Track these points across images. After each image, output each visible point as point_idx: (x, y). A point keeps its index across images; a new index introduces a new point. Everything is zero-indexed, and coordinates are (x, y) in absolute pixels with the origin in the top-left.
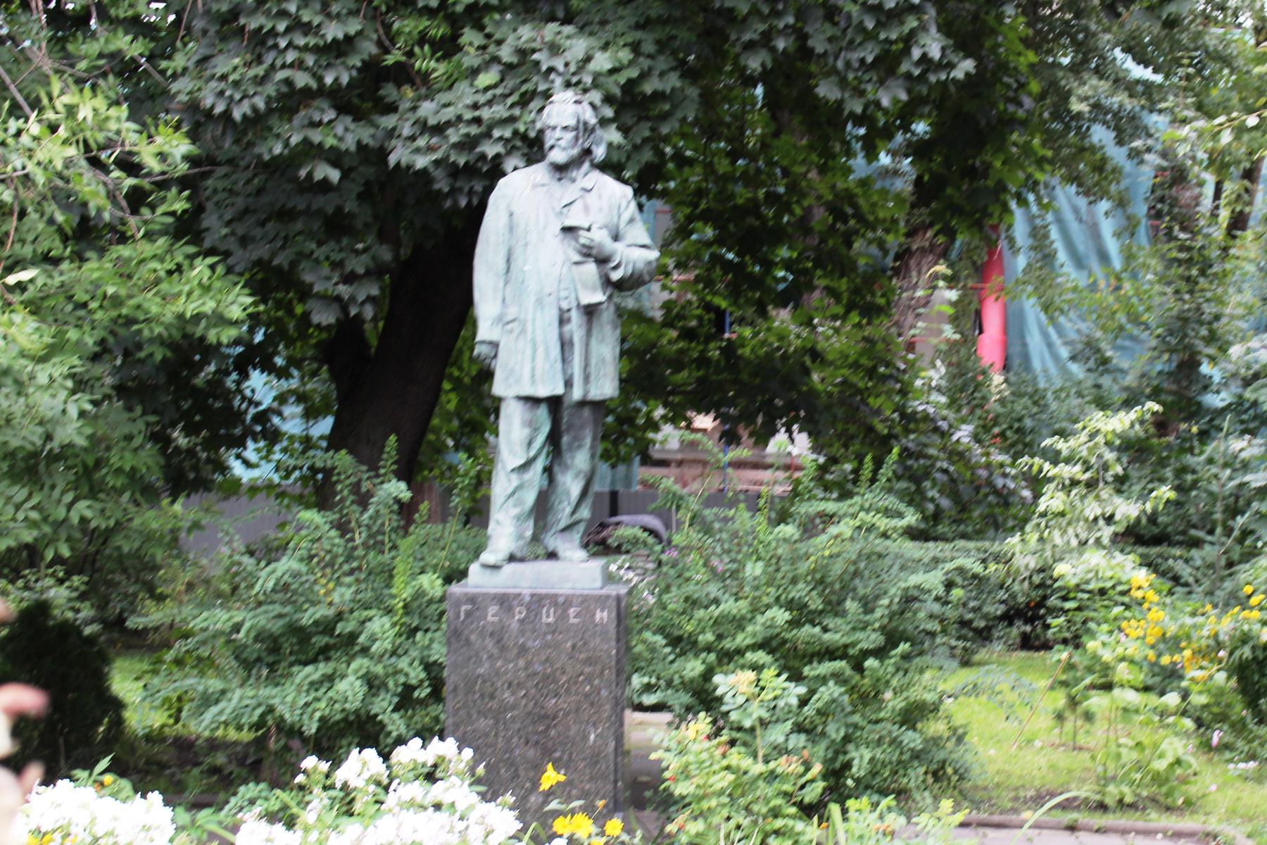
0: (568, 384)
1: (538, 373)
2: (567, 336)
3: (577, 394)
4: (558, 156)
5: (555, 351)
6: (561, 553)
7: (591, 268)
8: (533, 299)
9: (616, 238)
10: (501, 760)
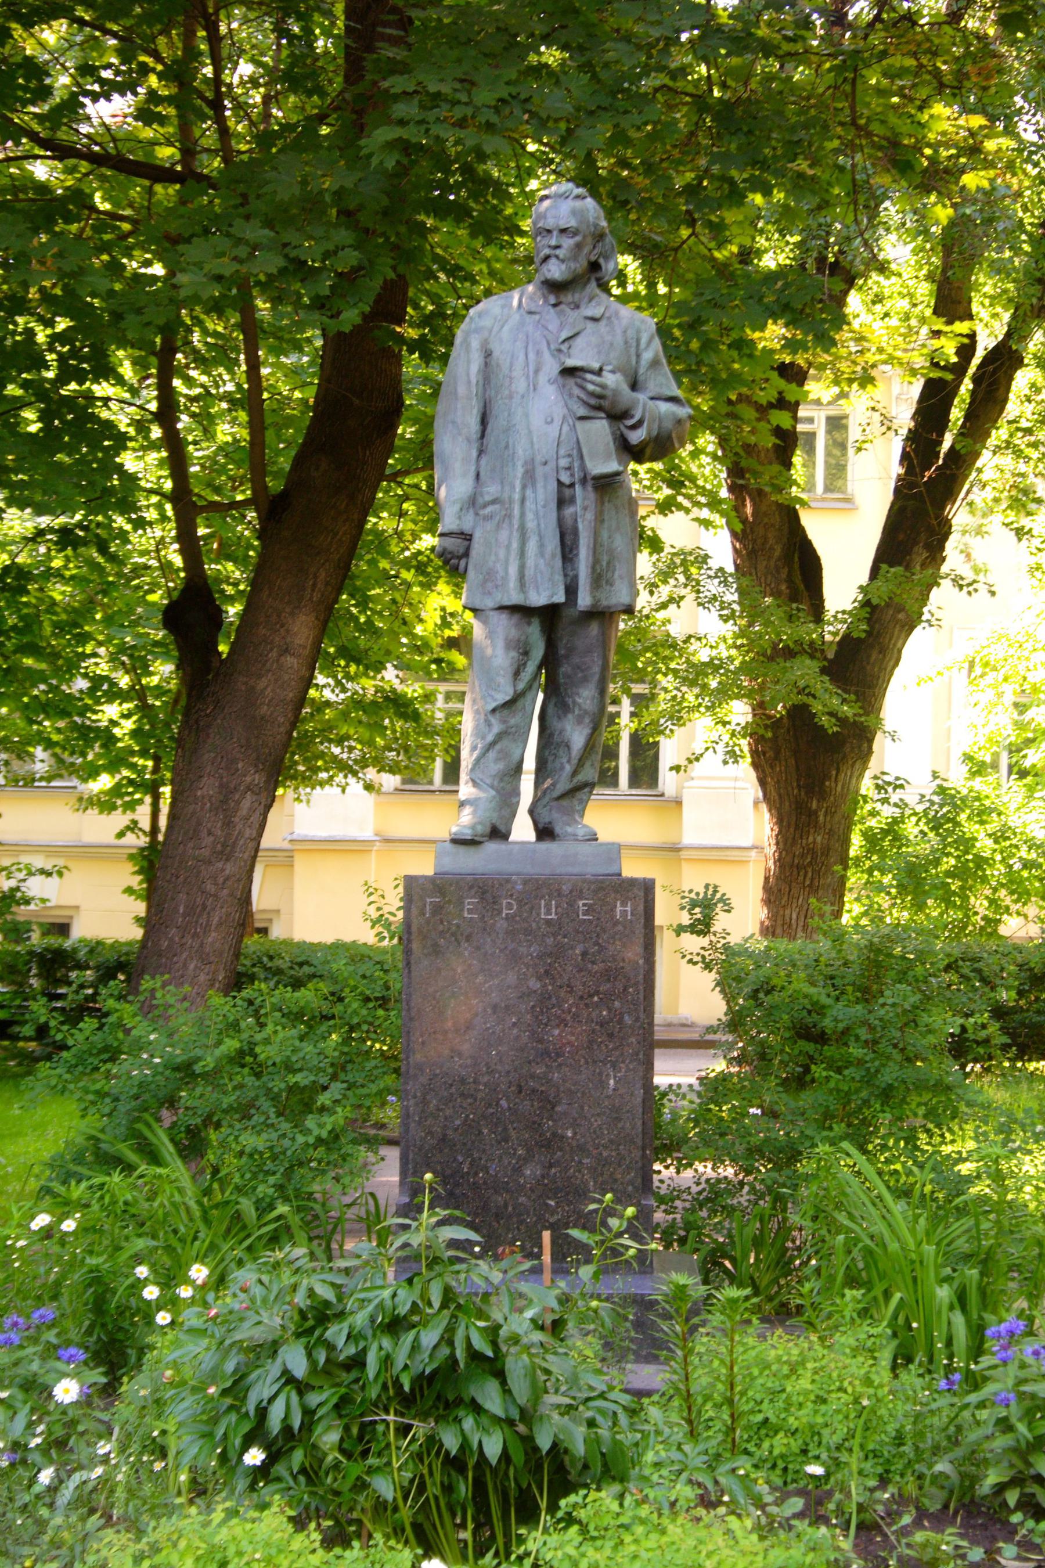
0: (571, 590)
1: (529, 572)
2: (569, 522)
3: (584, 600)
4: (555, 271)
5: (553, 544)
6: (558, 830)
7: (601, 428)
8: (520, 471)
9: (634, 386)
10: (484, 1116)
